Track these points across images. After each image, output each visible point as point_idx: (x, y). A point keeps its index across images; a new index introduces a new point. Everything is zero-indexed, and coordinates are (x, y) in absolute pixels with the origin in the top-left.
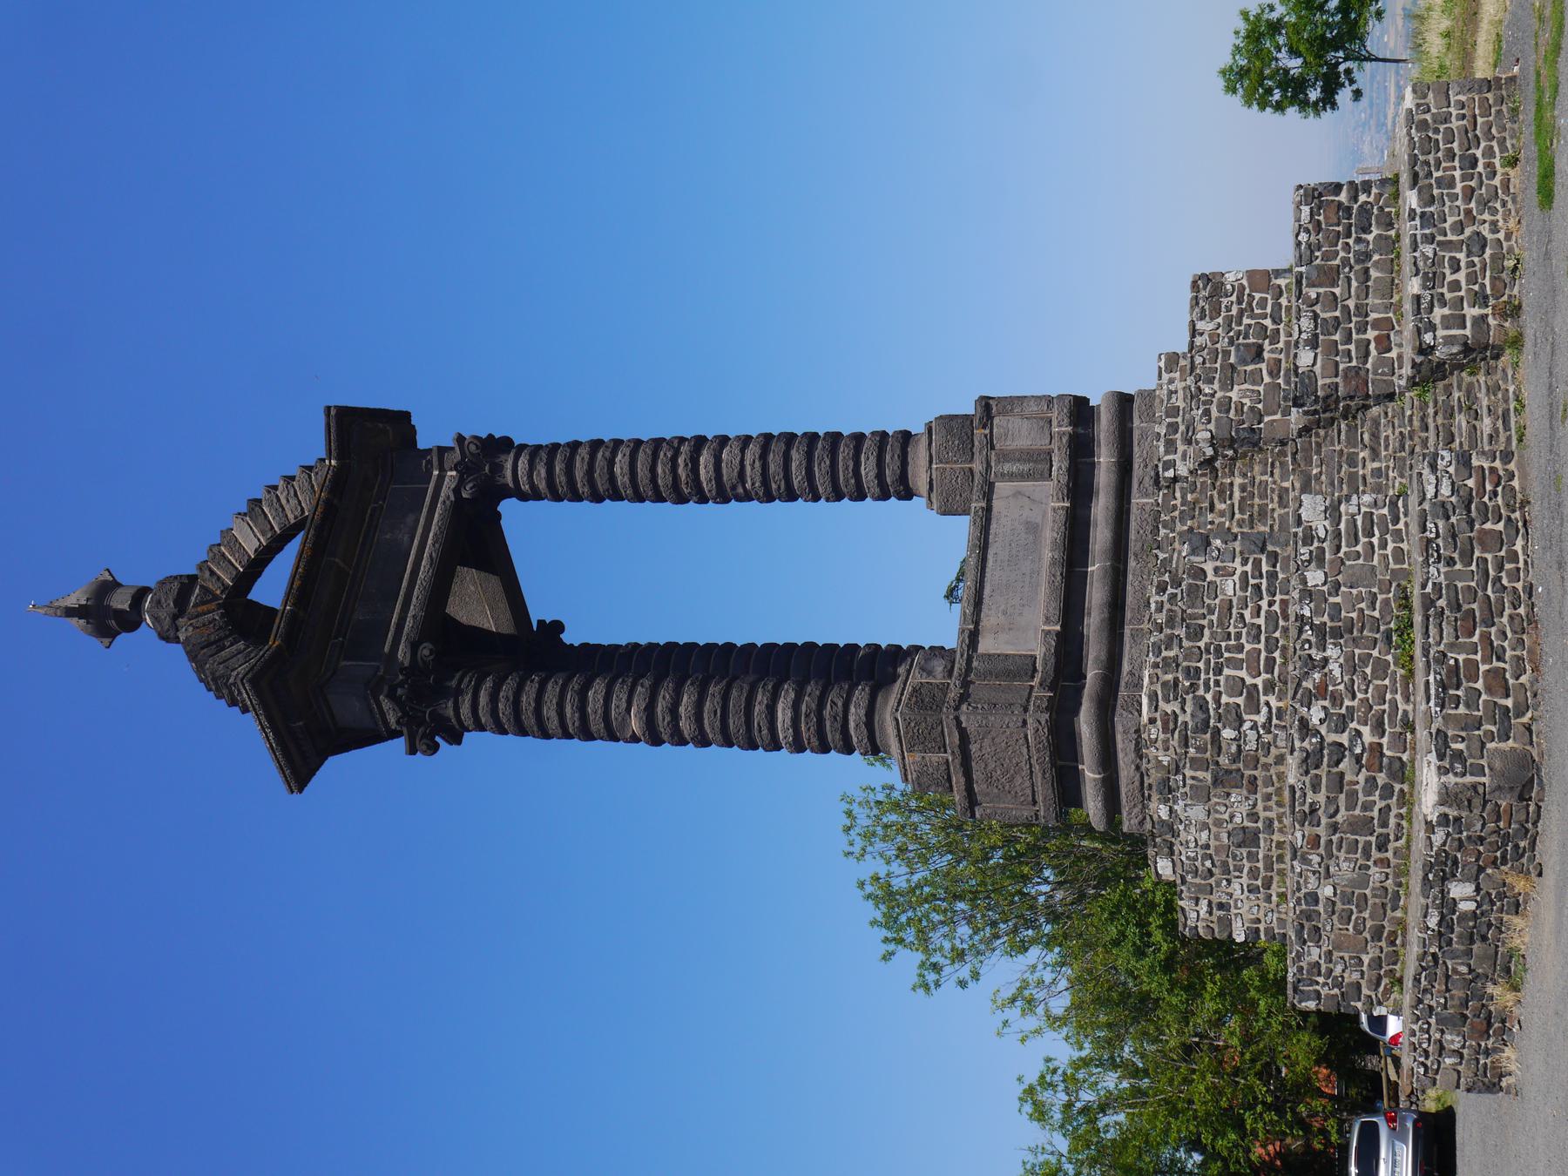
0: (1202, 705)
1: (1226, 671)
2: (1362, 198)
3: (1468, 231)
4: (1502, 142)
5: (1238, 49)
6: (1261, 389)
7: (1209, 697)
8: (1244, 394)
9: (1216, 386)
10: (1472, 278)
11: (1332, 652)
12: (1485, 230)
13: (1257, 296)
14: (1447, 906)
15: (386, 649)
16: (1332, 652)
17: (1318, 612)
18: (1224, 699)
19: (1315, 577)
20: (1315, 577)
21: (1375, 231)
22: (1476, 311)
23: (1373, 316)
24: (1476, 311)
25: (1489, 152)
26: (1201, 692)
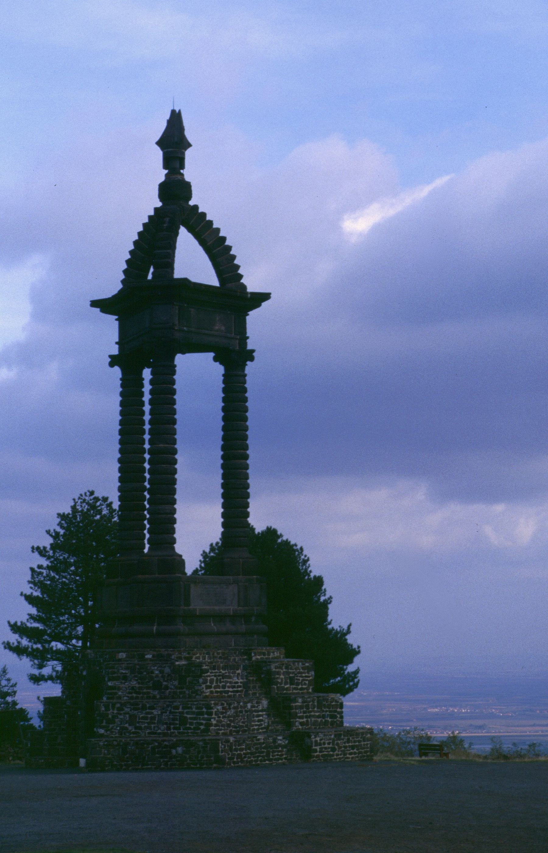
0: (207, 671)
1: (215, 678)
2: (338, 716)
3: (336, 747)
4: (357, 757)
5: (385, 734)
6: (283, 685)
7: (209, 674)
8: (282, 679)
9: (284, 670)
10: (326, 748)
11: (233, 711)
12: (336, 752)
13: (307, 682)
14: (174, 746)
15: (147, 374)
16: (233, 711)
17: (241, 707)
18: (209, 678)
19: (249, 705)
20: (249, 705)
21: (330, 720)
22: (318, 750)
23: (309, 720)
24: (318, 750)
25: (355, 753)
26: (210, 671)
